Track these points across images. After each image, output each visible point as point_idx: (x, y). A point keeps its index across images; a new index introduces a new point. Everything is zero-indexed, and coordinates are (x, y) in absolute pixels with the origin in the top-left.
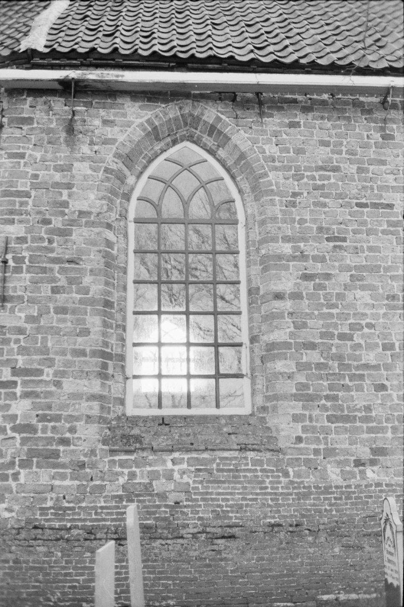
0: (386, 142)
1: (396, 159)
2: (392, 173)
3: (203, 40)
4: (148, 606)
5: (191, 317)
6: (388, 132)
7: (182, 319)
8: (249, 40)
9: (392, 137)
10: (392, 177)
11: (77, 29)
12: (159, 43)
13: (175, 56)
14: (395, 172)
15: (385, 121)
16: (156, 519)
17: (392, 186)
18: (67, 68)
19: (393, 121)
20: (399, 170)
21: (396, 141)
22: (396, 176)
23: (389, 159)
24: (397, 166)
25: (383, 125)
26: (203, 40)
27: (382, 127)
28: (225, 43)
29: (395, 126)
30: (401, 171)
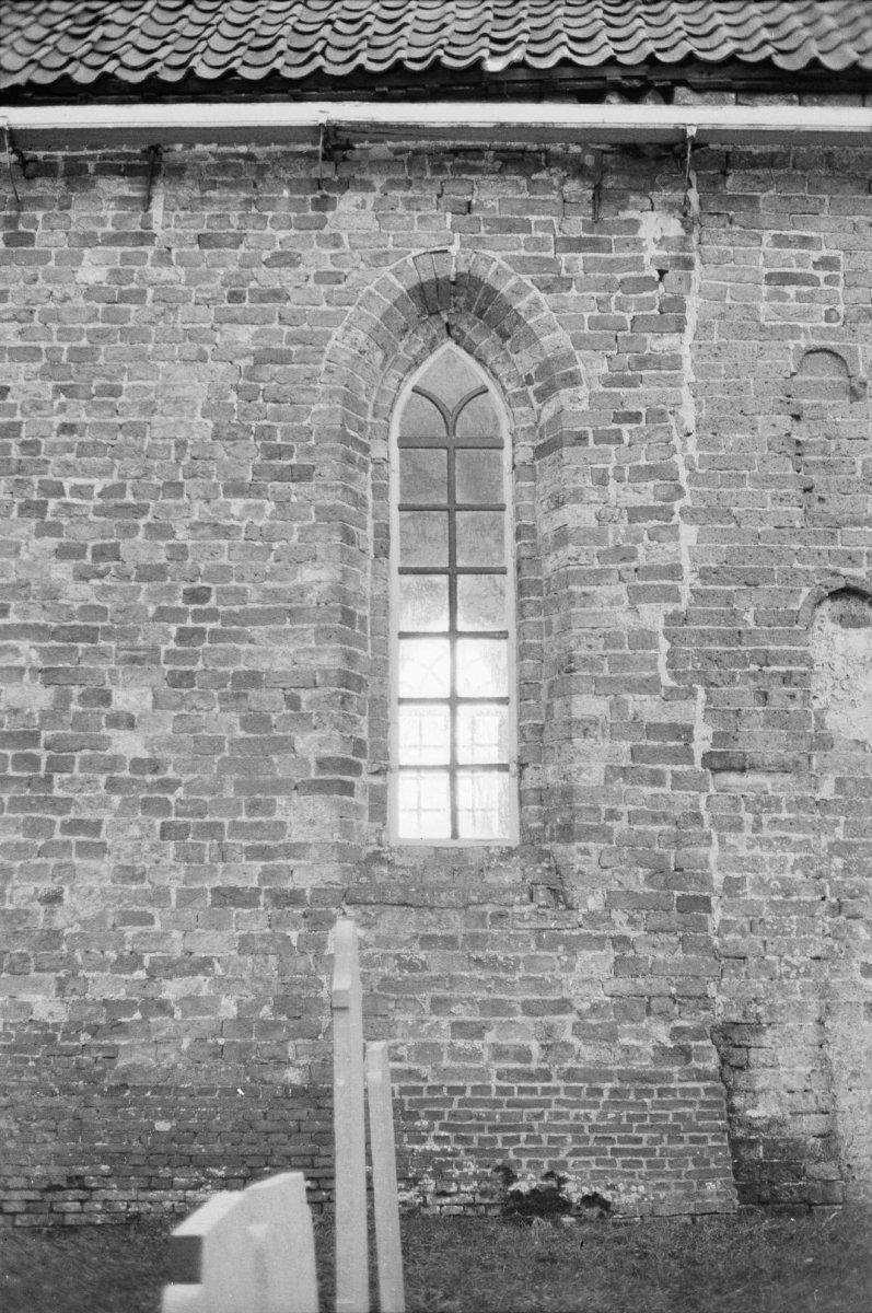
0: (13, 249)
1: (28, 287)
2: (15, 319)
3: (548, 40)
4: (262, 1310)
5: (460, 563)
6: (21, 228)
7: (435, 586)
8: (726, 32)
9: (28, 239)
10: (14, 327)
11: (360, 19)
12: (290, 48)
13: (768, 61)
14: (23, 315)
15: (19, 204)
16: (23, 1243)
17: (11, 349)
18: (707, 96)
19: (38, 202)
20: (32, 312)
21: (36, 248)
22: (24, 325)
23: (13, 288)
24: (27, 304)
25: (14, 213)
26: (548, 40)
27: (10, 217)
28: (133, 42)
29: (40, 215)
30: (36, 315)
